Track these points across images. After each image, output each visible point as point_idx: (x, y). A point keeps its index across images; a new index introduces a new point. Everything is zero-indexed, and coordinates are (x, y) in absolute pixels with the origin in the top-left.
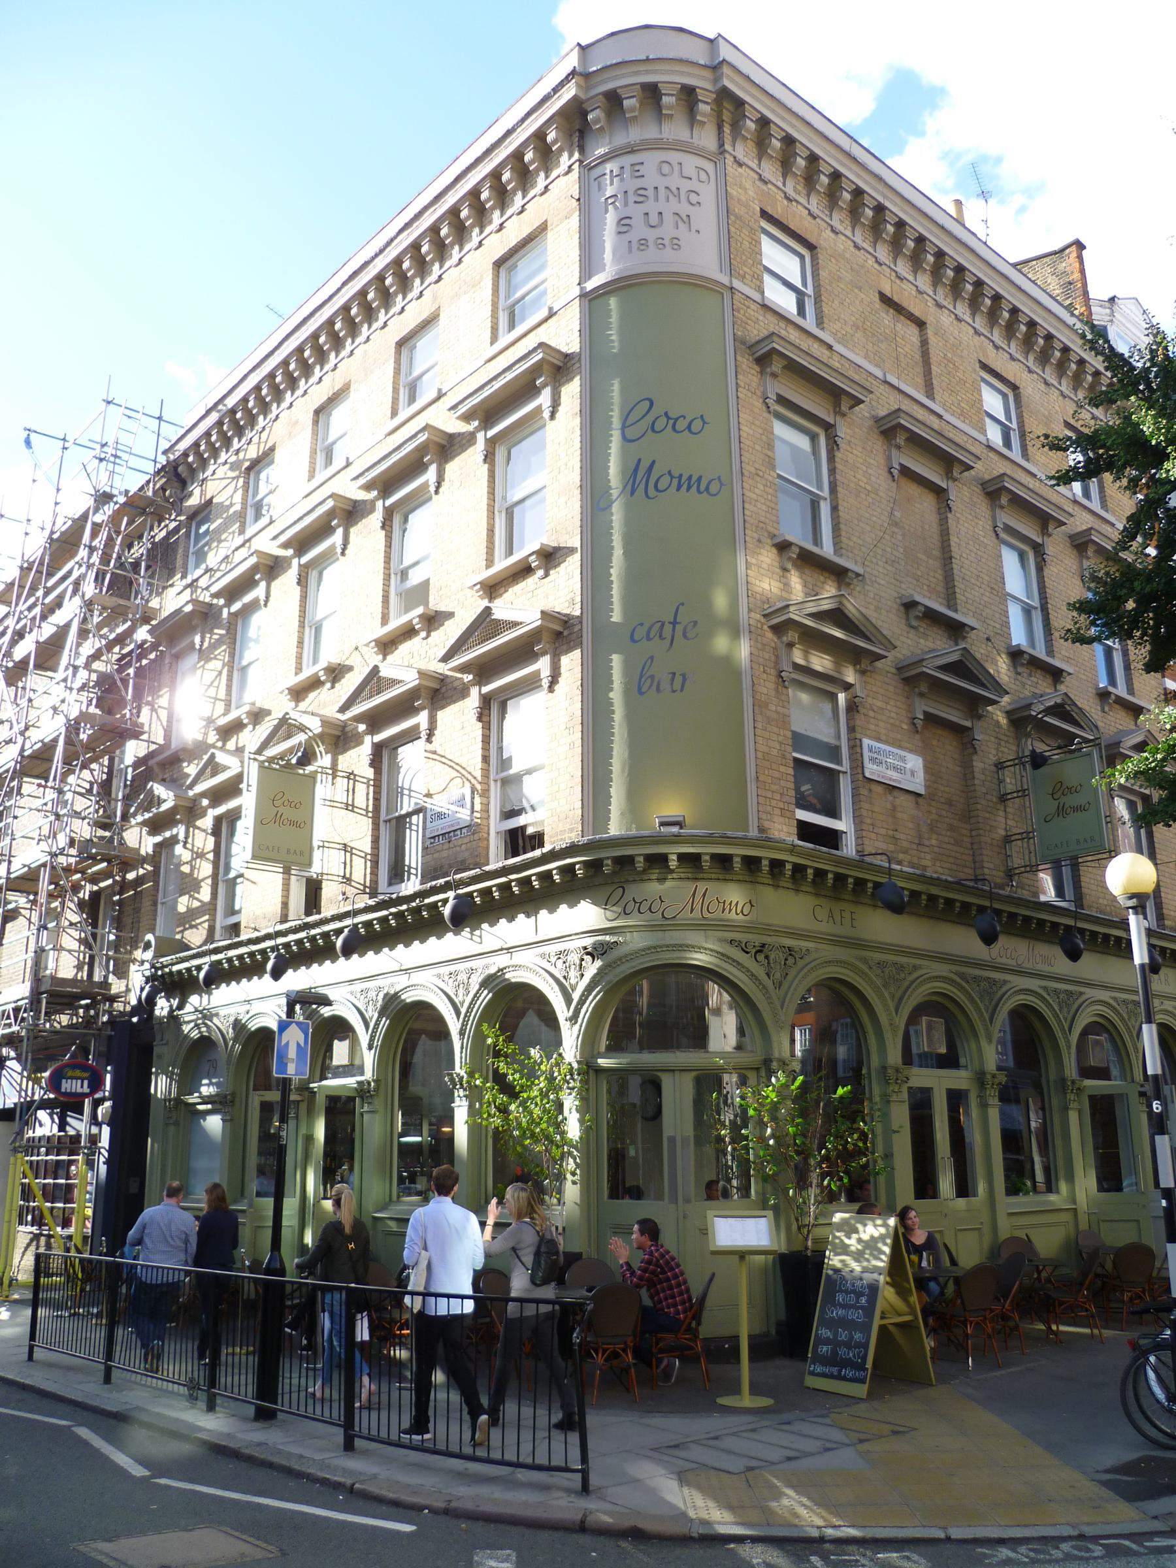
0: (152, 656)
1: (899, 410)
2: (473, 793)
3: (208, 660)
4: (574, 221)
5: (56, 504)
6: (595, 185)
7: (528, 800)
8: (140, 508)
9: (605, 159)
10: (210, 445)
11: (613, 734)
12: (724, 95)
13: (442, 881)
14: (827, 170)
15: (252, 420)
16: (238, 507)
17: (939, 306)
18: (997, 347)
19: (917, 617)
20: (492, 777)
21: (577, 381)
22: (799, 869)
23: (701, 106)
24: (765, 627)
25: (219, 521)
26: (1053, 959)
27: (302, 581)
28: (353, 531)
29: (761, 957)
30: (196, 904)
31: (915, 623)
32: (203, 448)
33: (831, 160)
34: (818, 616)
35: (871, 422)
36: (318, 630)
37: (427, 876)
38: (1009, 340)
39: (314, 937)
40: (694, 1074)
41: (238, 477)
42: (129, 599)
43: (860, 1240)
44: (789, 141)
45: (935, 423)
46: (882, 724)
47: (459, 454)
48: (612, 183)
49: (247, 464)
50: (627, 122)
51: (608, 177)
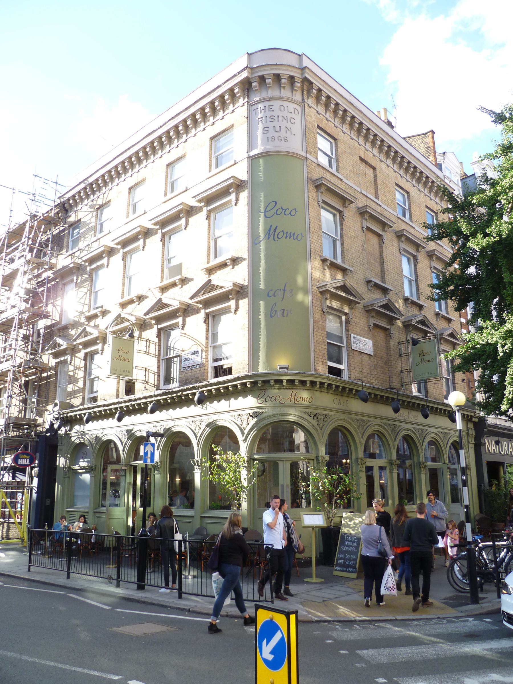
0: (53, 283)
2: (202, 351)
3: (80, 287)
4: (245, 126)
6: (253, 113)
8: (48, 222)
9: (258, 102)
10: (81, 197)
12: (305, 80)
13: (191, 386)
14: (342, 109)
15: (99, 188)
16: (93, 224)
17: (381, 161)
18: (402, 177)
19: (371, 286)
20: (209, 345)
21: (246, 191)
22: (330, 385)
23: (296, 84)
25: (84, 229)
26: (418, 417)
29: (315, 418)
30: (76, 388)
31: (370, 289)
34: (336, 288)
35: (356, 209)
36: (130, 279)
38: (406, 174)
39: (134, 405)
40: (291, 462)
41: (93, 212)
42: (40, 258)
43: (354, 523)
44: (328, 97)
45: (378, 209)
46: (358, 328)
48: (261, 113)
49: (97, 206)
50: (267, 88)
51: (259, 110)
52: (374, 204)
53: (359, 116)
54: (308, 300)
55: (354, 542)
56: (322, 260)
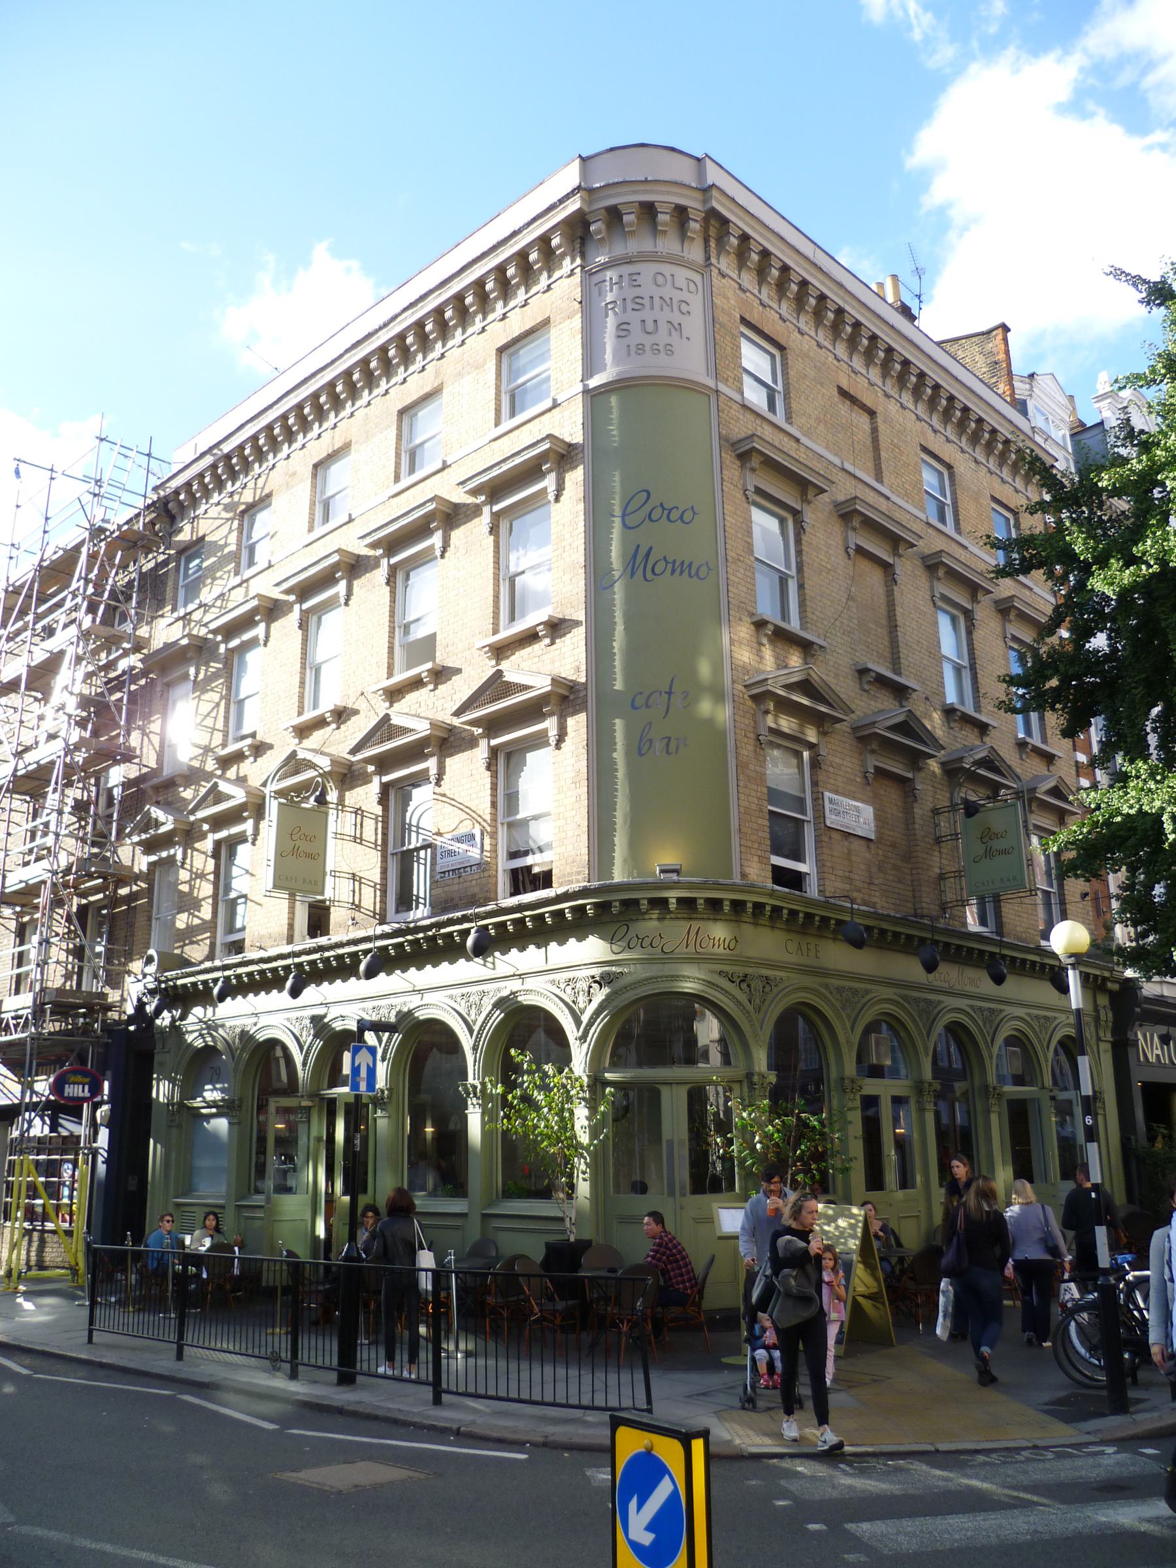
0: (143, 682)
2: (482, 834)
3: (204, 691)
4: (577, 322)
5: (45, 532)
6: (595, 290)
7: (534, 841)
8: (131, 543)
9: (605, 267)
12: (712, 215)
13: (459, 914)
14: (797, 279)
15: (247, 466)
16: (233, 548)
17: (887, 396)
18: (935, 431)
19: (869, 682)
22: (776, 910)
23: (692, 225)
27: (303, 625)
29: (744, 986)
30: (196, 921)
31: (866, 687)
32: (195, 487)
35: (831, 507)
36: (318, 671)
37: (440, 905)
38: (945, 424)
39: (328, 958)
40: (688, 1087)
41: (232, 519)
42: (113, 626)
44: (765, 254)
45: (883, 505)
46: (839, 778)
47: (465, 523)
48: (611, 290)
49: (242, 507)
50: (626, 235)
52: (872, 494)
54: (724, 714)
56: (753, 623)
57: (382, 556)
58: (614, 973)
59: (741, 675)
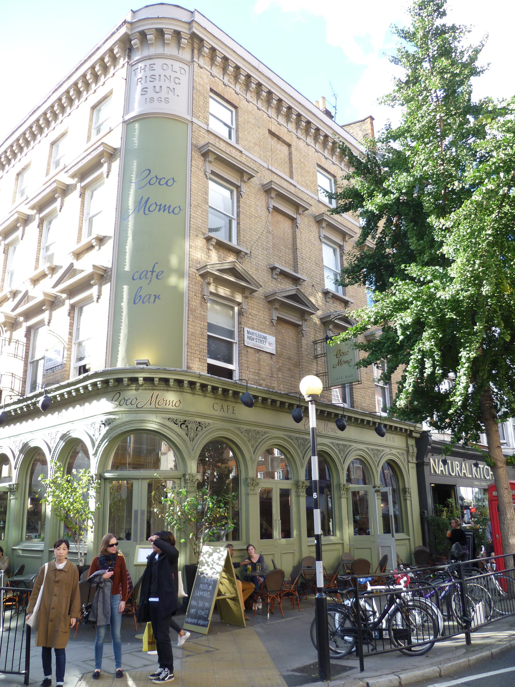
1: (272, 181)
6: (133, 73)
11: (121, 322)
12: (194, 36)
18: (326, 158)
19: (276, 274)
20: (73, 342)
21: (119, 159)
22: (203, 386)
23: (183, 40)
24: (197, 275)
26: (371, 436)
28: (27, 228)
29: (183, 426)
31: (275, 277)
33: (246, 69)
35: (260, 186)
38: (332, 156)
45: (292, 189)
46: (255, 321)
51: (139, 69)
52: (286, 183)
53: (268, 84)
54: (184, 284)
55: (209, 585)
56: (205, 238)
57: (36, 214)
58: (111, 419)
59: (195, 264)
